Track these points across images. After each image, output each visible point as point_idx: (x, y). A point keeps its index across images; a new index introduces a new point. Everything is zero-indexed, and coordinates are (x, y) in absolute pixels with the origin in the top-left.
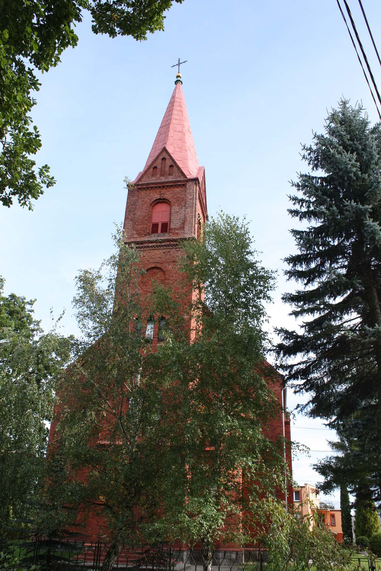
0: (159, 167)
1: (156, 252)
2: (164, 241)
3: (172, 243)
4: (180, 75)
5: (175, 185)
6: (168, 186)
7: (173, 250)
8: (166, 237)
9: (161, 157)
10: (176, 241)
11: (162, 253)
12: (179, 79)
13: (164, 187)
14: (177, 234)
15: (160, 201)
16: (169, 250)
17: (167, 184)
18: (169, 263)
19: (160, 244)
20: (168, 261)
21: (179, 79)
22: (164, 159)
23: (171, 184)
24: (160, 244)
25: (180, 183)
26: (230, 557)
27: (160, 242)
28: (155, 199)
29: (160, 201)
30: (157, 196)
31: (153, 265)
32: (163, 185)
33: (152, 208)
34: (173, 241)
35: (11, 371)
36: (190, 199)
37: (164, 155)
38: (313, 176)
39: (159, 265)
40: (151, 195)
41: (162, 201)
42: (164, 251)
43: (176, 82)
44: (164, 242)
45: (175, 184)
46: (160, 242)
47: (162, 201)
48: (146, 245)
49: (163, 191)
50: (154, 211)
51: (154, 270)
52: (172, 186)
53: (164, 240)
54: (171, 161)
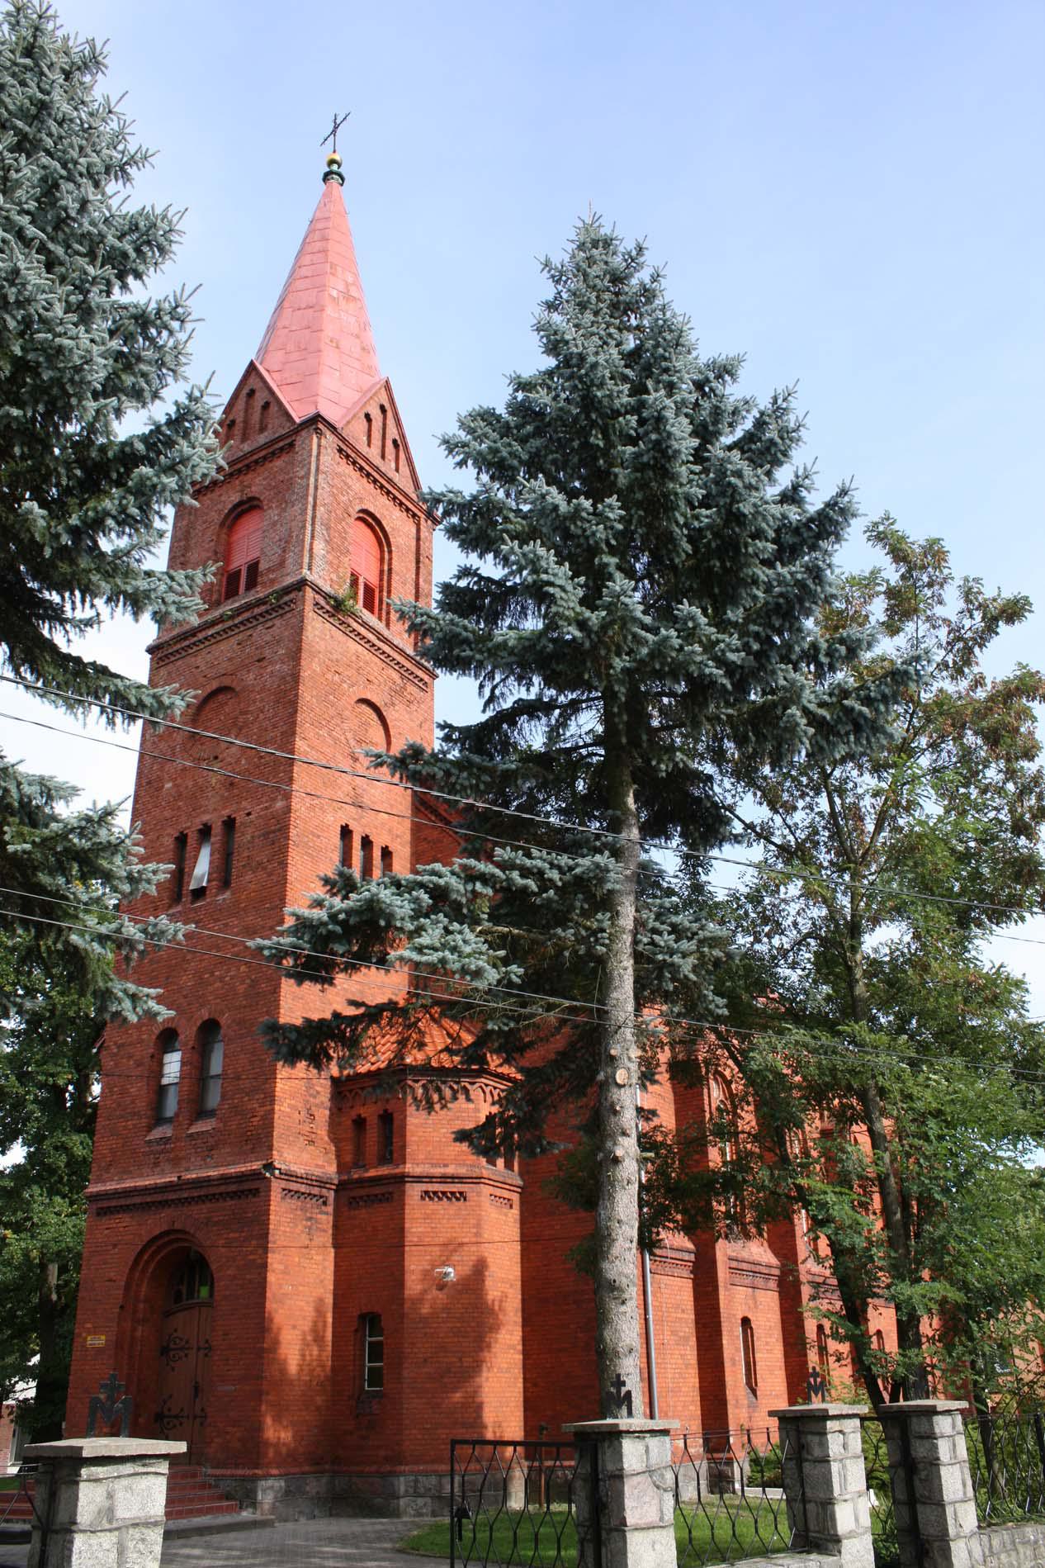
0: (240, 420)
1: (223, 646)
2: (238, 612)
3: (257, 611)
4: (337, 157)
5: (273, 453)
6: (256, 462)
7: (260, 627)
8: (260, 592)
9: (245, 391)
10: (265, 603)
11: (235, 647)
12: (335, 167)
13: (248, 466)
14: (273, 581)
15: (244, 507)
16: (249, 633)
17: (255, 457)
18: (246, 667)
19: (230, 623)
20: (247, 661)
21: (335, 167)
22: (252, 393)
23: (263, 453)
24: (230, 623)
25: (281, 444)
26: (440, 1492)
27: (232, 617)
28: (230, 506)
29: (244, 507)
30: (235, 498)
31: (215, 685)
32: (246, 462)
33: (229, 535)
34: (258, 606)
35: (771, 996)
36: (302, 478)
37: (253, 382)
38: (377, 336)
39: (226, 682)
40: (223, 498)
41: (247, 506)
42: (240, 637)
43: (327, 177)
44: (238, 615)
45: (271, 450)
46: (232, 617)
47: (247, 506)
48: (201, 636)
49: (247, 479)
50: (235, 538)
51: (221, 698)
52: (265, 458)
53: (238, 609)
54: (266, 393)
